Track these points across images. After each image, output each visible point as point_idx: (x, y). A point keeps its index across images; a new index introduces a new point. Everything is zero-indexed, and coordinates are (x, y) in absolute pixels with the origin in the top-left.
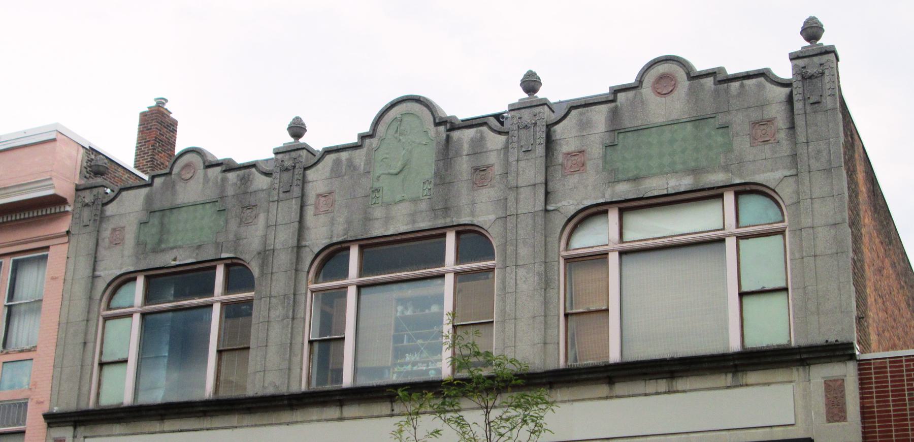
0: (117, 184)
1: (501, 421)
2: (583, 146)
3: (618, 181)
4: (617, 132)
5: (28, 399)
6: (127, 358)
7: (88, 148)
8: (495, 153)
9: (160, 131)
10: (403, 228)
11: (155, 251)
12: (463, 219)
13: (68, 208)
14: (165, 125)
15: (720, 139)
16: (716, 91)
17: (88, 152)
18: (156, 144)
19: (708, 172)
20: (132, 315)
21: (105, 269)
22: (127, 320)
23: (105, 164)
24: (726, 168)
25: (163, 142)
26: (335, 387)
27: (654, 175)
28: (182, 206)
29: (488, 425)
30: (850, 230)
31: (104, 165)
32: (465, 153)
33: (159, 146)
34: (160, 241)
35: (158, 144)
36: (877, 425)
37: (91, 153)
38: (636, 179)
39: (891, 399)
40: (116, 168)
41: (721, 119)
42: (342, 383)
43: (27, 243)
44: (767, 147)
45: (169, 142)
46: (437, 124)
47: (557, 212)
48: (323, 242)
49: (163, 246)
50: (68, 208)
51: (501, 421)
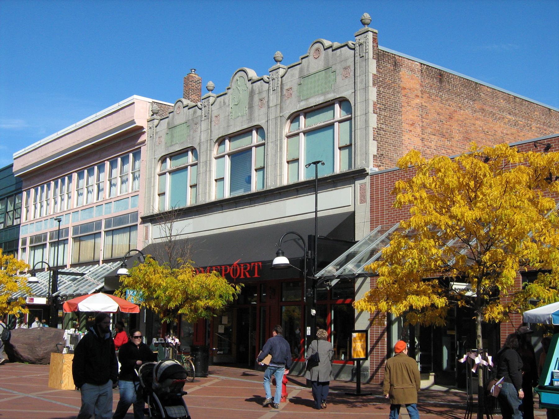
0: (85, 279)
1: (555, 230)
3: (302, 101)
8: (265, 92)
11: (172, 146)
13: (145, 130)
16: (333, 54)
19: (328, 93)
20: (299, 134)
22: (329, 132)
24: (334, 92)
26: (249, 193)
29: (152, 186)
32: (257, 93)
34: (172, 141)
38: (307, 99)
41: (333, 69)
42: (251, 190)
44: (347, 79)
46: (249, 81)
49: (173, 143)
51: (555, 230)
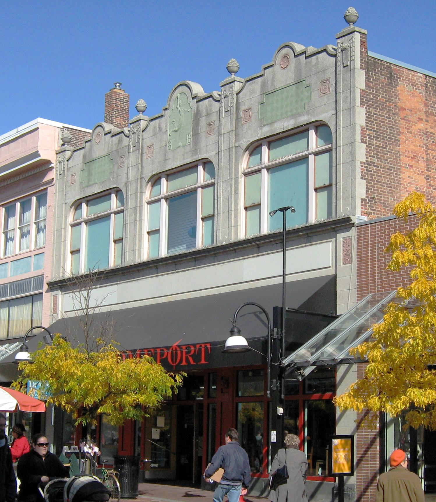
2: (251, 105)
3: (265, 125)
4: (264, 94)
5: (43, 275)
6: (80, 249)
7: (62, 127)
8: (215, 114)
9: (116, 104)
10: (179, 164)
12: (203, 155)
13: (52, 165)
14: (120, 100)
15: (306, 94)
16: (306, 63)
17: (63, 130)
18: (113, 113)
21: (69, 198)
23: (69, 136)
24: (308, 113)
25: (118, 110)
27: (279, 120)
28: (278, 54)
30: (298, 424)
31: (68, 137)
32: (204, 115)
33: (116, 113)
34: (89, 181)
35: (115, 113)
36: (363, 471)
37: (64, 130)
38: (271, 124)
39: (370, 497)
40: (84, 134)
43: (24, 197)
44: (326, 97)
45: (123, 109)
47: (239, 147)
48: (150, 174)
50: (52, 165)
